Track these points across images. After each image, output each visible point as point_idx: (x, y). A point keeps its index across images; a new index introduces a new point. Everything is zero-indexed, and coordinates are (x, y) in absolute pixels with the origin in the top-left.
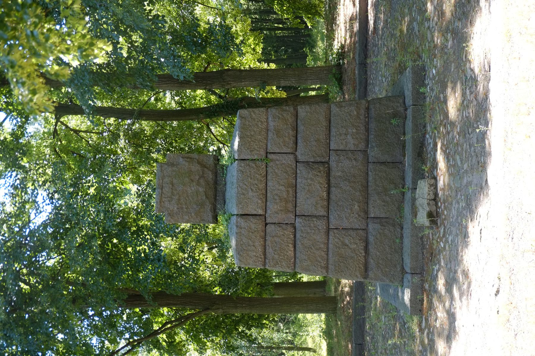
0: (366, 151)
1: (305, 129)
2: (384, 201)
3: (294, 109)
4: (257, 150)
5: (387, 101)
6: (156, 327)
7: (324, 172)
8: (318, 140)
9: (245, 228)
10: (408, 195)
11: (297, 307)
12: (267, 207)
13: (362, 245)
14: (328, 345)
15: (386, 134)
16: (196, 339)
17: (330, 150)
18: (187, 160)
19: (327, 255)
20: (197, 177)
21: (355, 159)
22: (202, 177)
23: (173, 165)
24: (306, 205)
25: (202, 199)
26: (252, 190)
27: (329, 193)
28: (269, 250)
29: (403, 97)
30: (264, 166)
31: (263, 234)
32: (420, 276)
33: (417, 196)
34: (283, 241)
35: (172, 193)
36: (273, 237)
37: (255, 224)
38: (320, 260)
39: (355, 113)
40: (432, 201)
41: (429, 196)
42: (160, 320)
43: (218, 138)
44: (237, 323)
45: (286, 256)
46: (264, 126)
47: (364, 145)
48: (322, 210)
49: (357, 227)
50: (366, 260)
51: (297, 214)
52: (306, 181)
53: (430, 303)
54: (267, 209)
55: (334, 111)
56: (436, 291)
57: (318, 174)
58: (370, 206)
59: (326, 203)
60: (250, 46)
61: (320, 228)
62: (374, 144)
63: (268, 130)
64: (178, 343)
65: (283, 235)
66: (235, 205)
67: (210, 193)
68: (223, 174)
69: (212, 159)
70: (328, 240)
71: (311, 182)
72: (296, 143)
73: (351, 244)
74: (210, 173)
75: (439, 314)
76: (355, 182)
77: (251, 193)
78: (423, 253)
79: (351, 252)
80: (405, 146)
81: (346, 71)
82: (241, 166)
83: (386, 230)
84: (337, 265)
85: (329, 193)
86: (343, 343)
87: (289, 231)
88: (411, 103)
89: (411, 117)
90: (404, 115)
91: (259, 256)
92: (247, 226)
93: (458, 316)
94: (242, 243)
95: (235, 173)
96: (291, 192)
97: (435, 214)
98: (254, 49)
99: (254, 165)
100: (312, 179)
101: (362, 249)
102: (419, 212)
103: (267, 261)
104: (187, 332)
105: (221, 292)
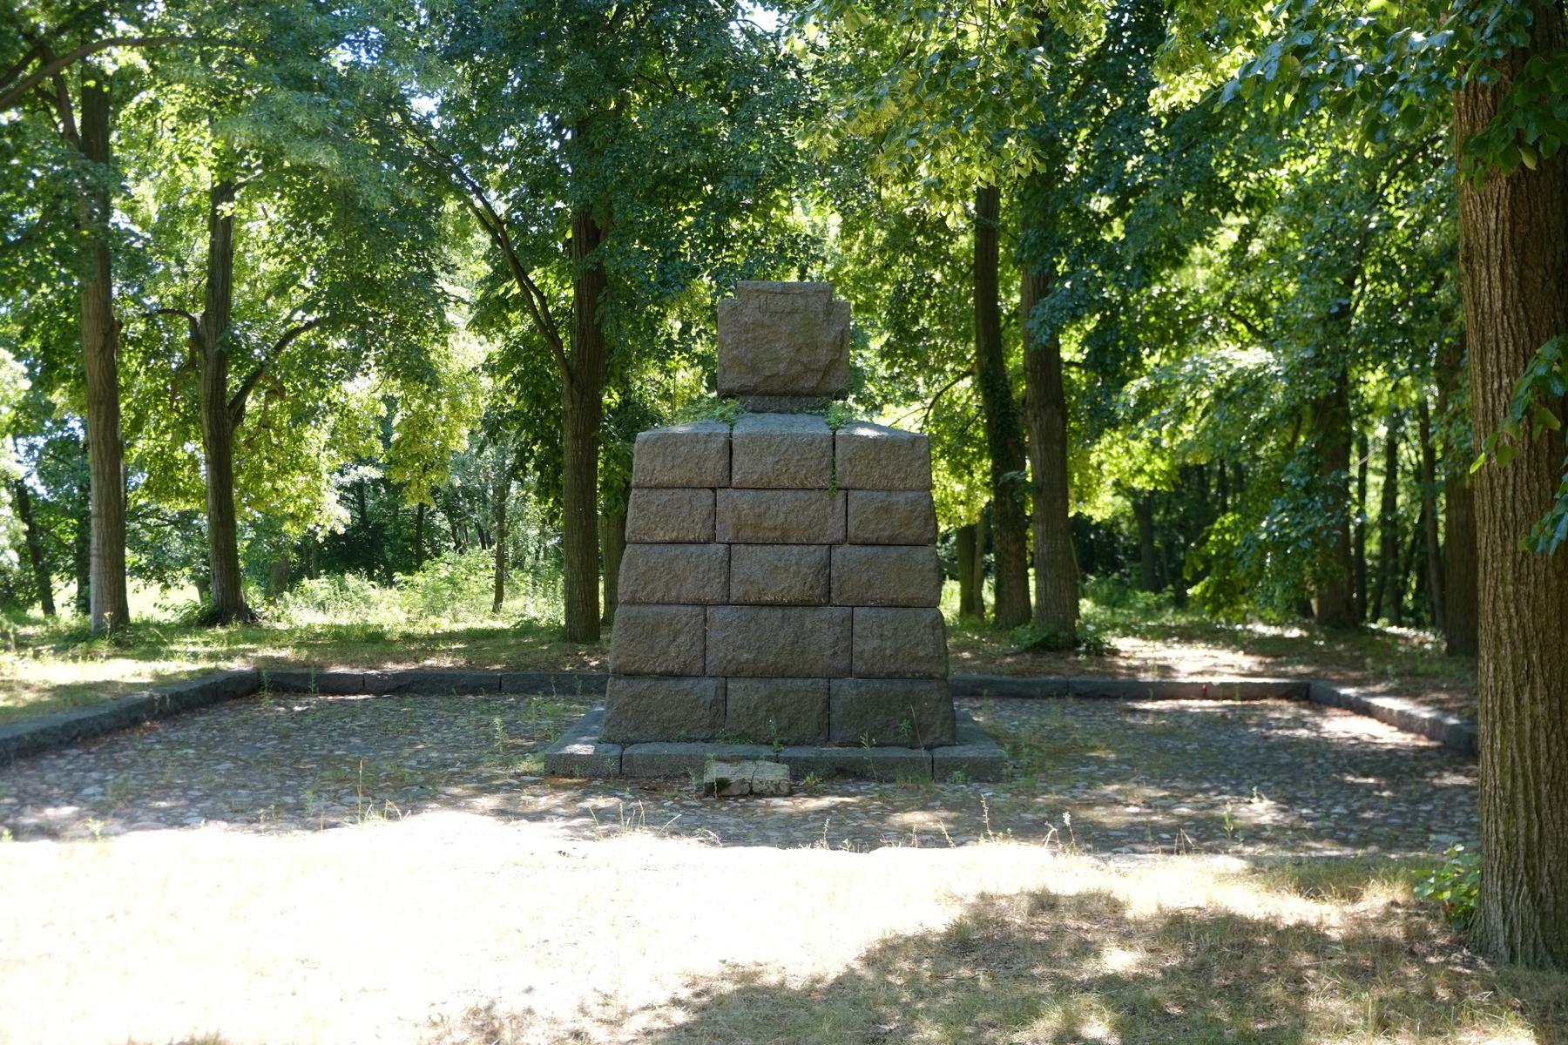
2: (756, 707)
6: (535, 275)
8: (870, 584)
10: (766, 751)
11: (577, 561)
13: (674, 666)
14: (502, 632)
16: (511, 357)
19: (657, 603)
20: (805, 360)
21: (835, 654)
22: (807, 368)
23: (828, 313)
27: (772, 605)
28: (665, 496)
30: (822, 484)
31: (695, 483)
35: (774, 313)
37: (713, 469)
39: (921, 654)
42: (550, 281)
44: (548, 439)
46: (897, 483)
48: (740, 593)
49: (709, 658)
53: (566, 788)
56: (585, 795)
58: (748, 682)
59: (753, 599)
60: (1149, 461)
64: (505, 318)
66: (749, 430)
72: (865, 544)
75: (543, 800)
77: (770, 460)
85: (772, 605)
86: (503, 656)
87: (701, 532)
93: (538, 825)
95: (809, 430)
97: (725, 793)
98: (1140, 471)
100: (797, 573)
104: (525, 338)
105: (609, 406)
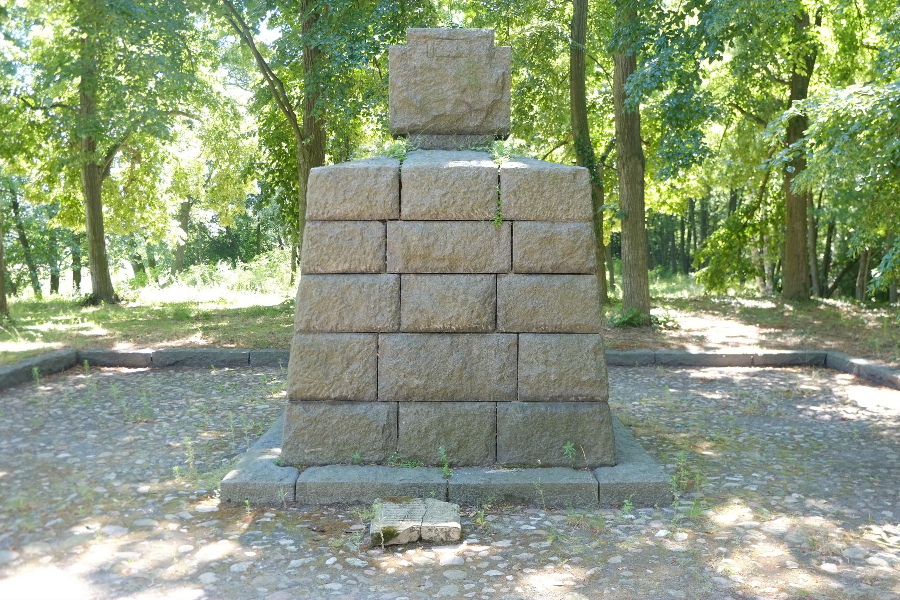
0: (516, 397)
1: (555, 288)
2: (427, 431)
3: (591, 269)
4: (516, 203)
5: (606, 434)
7: (478, 324)
8: (535, 312)
9: (376, 183)
10: (436, 477)
12: (416, 224)
15: (548, 434)
17: (518, 334)
18: (500, 81)
19: (332, 332)
20: (470, 100)
21: (502, 379)
22: (471, 109)
23: (491, 57)
24: (418, 292)
25: (432, 109)
26: (445, 195)
27: (441, 333)
28: (337, 228)
29: (613, 463)
30: (488, 216)
32: (292, 499)
33: (430, 502)
34: (355, 253)
35: (440, 58)
36: (361, 234)
37: (383, 203)
38: (323, 318)
39: (585, 379)
40: (418, 536)
41: (427, 530)
43: (549, 158)
45: (327, 258)
47: (527, 395)
48: (411, 322)
50: (324, 400)
51: (403, 277)
52: (462, 291)
54: (412, 223)
55: (588, 341)
57: (475, 314)
58: (419, 407)
61: (378, 319)
62: (529, 412)
63: (553, 222)
65: (365, 253)
66: (417, 165)
67: (442, 123)
68: (476, 146)
69: (502, 126)
70: (357, 332)
71: (460, 301)
72: (529, 274)
73: (351, 373)
74: (478, 123)
76: (461, 379)
77: (438, 193)
78: (330, 506)
79: (336, 374)
80: (525, 468)
81: (644, 332)
82: (487, 175)
83: (375, 435)
84: (313, 349)
85: (441, 333)
88: (604, 482)
89: (577, 482)
90: (581, 465)
91: (327, 210)
92: (380, 188)
94: (350, 178)
96: (442, 265)
97: (391, 543)
98: (664, 203)
99: (489, 197)
100: (465, 302)
101: (341, 393)
102: (400, 507)
103: (319, 225)
